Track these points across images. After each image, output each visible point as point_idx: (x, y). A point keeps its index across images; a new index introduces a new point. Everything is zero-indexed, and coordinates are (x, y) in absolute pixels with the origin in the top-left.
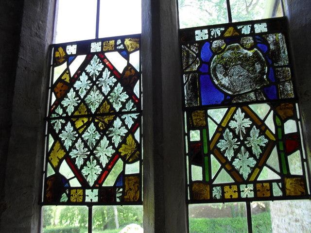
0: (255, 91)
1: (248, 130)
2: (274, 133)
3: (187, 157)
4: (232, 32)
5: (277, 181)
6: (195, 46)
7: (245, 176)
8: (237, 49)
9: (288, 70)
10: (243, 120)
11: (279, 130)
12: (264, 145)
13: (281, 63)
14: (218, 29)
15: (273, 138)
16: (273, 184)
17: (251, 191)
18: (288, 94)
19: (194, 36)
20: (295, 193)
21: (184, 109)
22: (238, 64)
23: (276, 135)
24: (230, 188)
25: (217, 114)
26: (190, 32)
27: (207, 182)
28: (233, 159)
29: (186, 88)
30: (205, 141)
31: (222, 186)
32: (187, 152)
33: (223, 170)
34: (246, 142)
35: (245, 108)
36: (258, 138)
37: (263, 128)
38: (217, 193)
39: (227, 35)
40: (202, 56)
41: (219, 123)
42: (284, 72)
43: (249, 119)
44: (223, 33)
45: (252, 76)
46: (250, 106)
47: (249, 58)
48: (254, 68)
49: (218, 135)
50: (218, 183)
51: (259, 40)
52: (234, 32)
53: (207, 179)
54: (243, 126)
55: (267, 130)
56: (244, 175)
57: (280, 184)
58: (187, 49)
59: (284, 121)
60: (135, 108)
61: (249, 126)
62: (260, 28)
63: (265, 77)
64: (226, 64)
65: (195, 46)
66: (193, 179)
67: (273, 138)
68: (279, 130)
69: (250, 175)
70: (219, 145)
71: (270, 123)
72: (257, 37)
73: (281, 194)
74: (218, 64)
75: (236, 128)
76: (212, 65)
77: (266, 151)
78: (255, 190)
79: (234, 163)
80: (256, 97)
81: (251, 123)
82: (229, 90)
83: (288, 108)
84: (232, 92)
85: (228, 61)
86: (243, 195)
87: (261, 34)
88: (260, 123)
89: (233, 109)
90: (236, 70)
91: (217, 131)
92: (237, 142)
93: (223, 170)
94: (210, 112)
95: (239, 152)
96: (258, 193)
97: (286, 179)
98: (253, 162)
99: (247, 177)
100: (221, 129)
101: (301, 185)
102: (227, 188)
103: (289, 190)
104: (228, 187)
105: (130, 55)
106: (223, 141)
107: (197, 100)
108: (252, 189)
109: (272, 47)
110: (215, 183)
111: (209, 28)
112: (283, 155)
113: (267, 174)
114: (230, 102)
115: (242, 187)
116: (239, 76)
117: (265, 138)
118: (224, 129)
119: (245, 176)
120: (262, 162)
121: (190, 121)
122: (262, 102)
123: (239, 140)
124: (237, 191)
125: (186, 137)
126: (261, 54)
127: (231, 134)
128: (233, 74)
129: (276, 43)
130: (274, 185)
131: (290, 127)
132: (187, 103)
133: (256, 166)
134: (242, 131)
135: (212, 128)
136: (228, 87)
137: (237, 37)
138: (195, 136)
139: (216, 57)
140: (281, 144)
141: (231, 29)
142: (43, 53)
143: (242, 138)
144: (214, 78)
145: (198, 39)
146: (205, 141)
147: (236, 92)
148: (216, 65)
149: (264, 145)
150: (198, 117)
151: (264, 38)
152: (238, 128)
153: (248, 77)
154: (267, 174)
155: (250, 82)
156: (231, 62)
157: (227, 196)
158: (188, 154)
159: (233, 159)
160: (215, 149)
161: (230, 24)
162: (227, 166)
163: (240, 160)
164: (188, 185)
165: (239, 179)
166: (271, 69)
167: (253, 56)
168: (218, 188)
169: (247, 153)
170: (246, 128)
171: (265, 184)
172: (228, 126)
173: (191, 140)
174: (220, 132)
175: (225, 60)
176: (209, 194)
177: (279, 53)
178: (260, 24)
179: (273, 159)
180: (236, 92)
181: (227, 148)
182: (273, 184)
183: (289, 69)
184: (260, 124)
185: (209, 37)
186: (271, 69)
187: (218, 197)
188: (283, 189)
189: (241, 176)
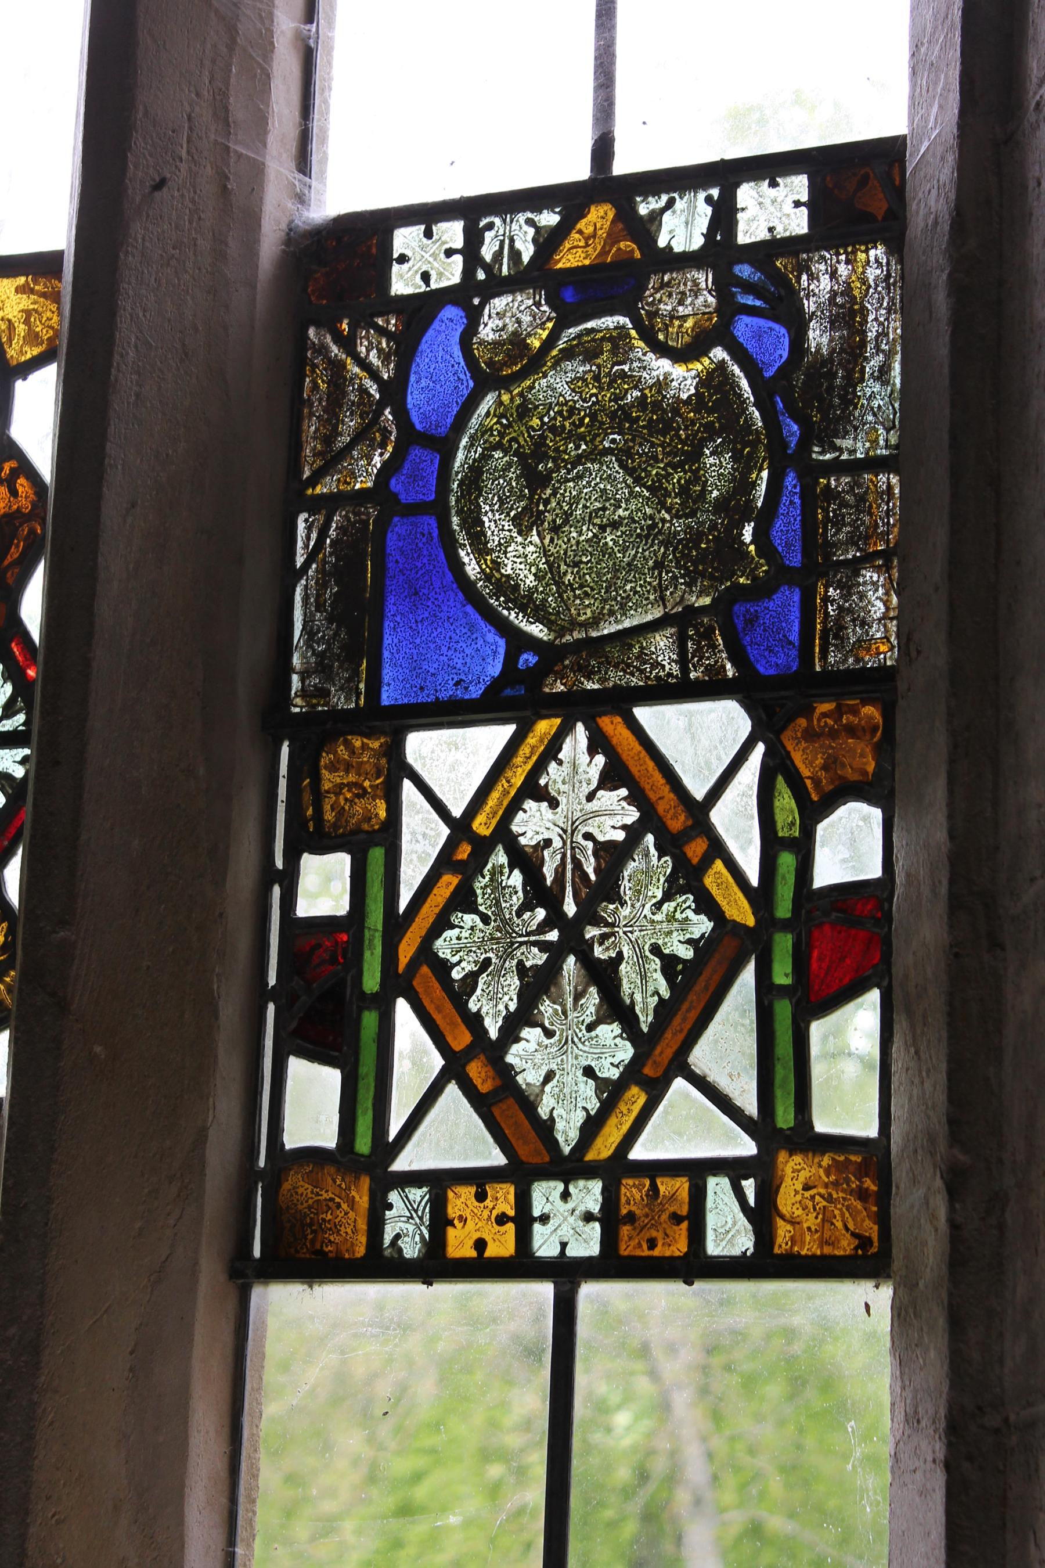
0: (681, 621)
1: (613, 856)
2: (754, 880)
3: (271, 1008)
4: (597, 241)
5: (734, 1169)
6: (382, 331)
7: (567, 1132)
8: (614, 351)
9: (890, 487)
10: (590, 797)
11: (787, 861)
12: (686, 953)
13: (855, 446)
14: (522, 217)
15: (740, 911)
16: (712, 1182)
17: (588, 1217)
18: (864, 644)
19: (383, 259)
20: (823, 1242)
21: (274, 720)
22: (608, 451)
23: (761, 897)
24: (481, 1197)
25: (453, 759)
26: (366, 237)
27: (366, 1157)
28: (511, 1029)
29: (306, 599)
30: (375, 917)
31: (440, 1182)
32: (272, 981)
33: (452, 1090)
34: (592, 932)
35: (613, 726)
36: (658, 906)
37: (696, 849)
38: (404, 1225)
39: (571, 257)
40: (414, 398)
41: (457, 811)
42: (862, 499)
43: (623, 792)
44: (549, 242)
45: (678, 525)
46: (643, 714)
47: (676, 412)
48: (696, 477)
49: (449, 882)
50: (416, 1166)
51: (749, 287)
52: (613, 238)
53: (363, 1145)
54: (588, 836)
55: (719, 865)
56: (560, 1125)
57: (749, 1186)
58: (335, 349)
59: (814, 811)
60: (21, 718)
61: (620, 836)
62: (772, 211)
63: (748, 533)
64: (539, 450)
65: (382, 331)
66: (291, 1141)
67: (740, 911)
68: (787, 861)
69: (592, 1126)
70: (444, 946)
71: (737, 823)
72: (744, 271)
73: (743, 1242)
74: (498, 446)
75: (548, 843)
76: (460, 456)
77: (695, 988)
78: (610, 1218)
79: (514, 1056)
80: (683, 661)
81: (632, 815)
82: (539, 614)
83: (851, 731)
84: (548, 623)
85: (553, 429)
86: (545, 1244)
87: (774, 247)
88: (677, 822)
89: (545, 727)
90: (597, 486)
91: (444, 861)
92: (544, 927)
93: (452, 1090)
94: (422, 747)
95: (547, 992)
96: (625, 1230)
97: (782, 1156)
98: (612, 1050)
99: (574, 1135)
100: (468, 847)
101: (862, 1195)
102: (461, 1200)
103: (793, 1222)
104: (467, 1192)
105: (19, 384)
106: (470, 919)
107: (356, 673)
108: (596, 1209)
109: (818, 337)
110: (402, 1164)
111: (473, 211)
112: (783, 1010)
113: (683, 1129)
114: (556, 684)
115: (545, 1195)
116: (602, 528)
117: (697, 912)
118: (483, 848)
119: (567, 1132)
120: (665, 1050)
121: (307, 797)
122: (711, 688)
123: (555, 918)
124: (535, 1219)
125: (277, 890)
126: (744, 384)
127: (516, 879)
128: (567, 516)
129: (847, 314)
130: (718, 1187)
131: (849, 846)
132: (303, 693)
133: (632, 1073)
134: (578, 865)
135: (422, 839)
136: (532, 591)
137: (629, 274)
138: (324, 887)
139: (488, 402)
140: (783, 944)
141: (599, 217)
142: (251, 284)
143: (570, 908)
144: (462, 538)
145: (403, 283)
146: (375, 917)
147: (574, 624)
148: (485, 457)
149: (686, 953)
150: (352, 778)
151: (780, 280)
152: (557, 843)
153: (651, 531)
154: (683, 1129)
155: (659, 565)
156: (570, 437)
157: (459, 1244)
158: (274, 995)
159: (511, 1029)
160: (425, 969)
161: (606, 186)
162: (476, 1070)
163: (549, 1034)
164: (261, 1174)
165: (530, 1151)
166: (790, 480)
167: (698, 402)
168: (417, 1194)
169: (593, 998)
170: (603, 849)
171: (666, 1186)
172: (504, 835)
173: (303, 910)
174: (457, 867)
175: (536, 422)
176: (362, 1225)
177: (854, 379)
178: (774, 184)
179: (727, 1047)
180: (574, 624)
181: (487, 962)
182: (712, 1182)
183: (894, 480)
184: (678, 825)
185: (468, 272)
186: (790, 480)
187: (411, 1249)
188: (762, 1216)
189: (546, 1128)
